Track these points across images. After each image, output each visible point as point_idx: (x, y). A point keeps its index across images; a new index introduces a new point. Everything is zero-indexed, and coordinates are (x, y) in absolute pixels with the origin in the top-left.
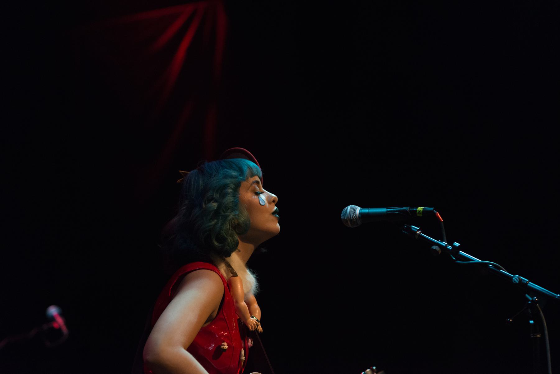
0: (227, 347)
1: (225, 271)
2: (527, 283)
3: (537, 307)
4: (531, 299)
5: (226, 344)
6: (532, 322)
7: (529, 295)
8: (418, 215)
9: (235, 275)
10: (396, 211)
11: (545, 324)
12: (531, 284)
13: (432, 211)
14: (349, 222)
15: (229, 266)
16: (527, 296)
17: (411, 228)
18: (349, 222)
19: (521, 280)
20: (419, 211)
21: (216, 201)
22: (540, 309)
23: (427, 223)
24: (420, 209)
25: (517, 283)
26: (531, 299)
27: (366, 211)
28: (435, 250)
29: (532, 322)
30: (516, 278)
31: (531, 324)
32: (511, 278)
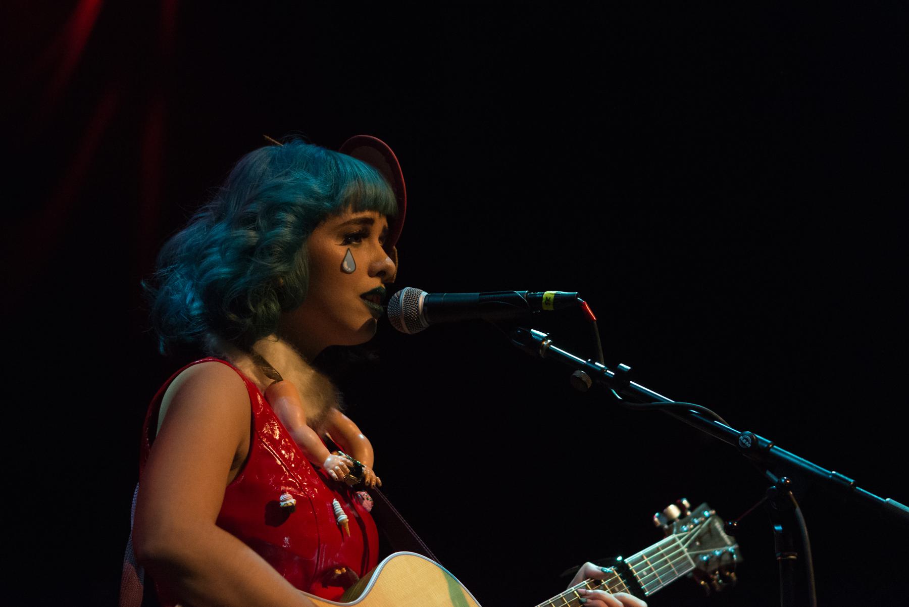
0: (293, 501)
1: (254, 372)
2: (768, 448)
3: (789, 496)
4: (776, 480)
5: (288, 495)
6: (778, 528)
7: (773, 473)
8: (545, 308)
9: (279, 379)
10: (500, 299)
11: (806, 532)
12: (778, 450)
13: (572, 299)
14: (403, 322)
15: (261, 362)
16: (769, 473)
17: (531, 334)
18: (403, 322)
19: (755, 442)
20: (548, 299)
21: (257, 229)
22: (794, 501)
23: (562, 321)
24: (549, 294)
25: (747, 448)
26: (776, 480)
27: (443, 297)
28: (580, 379)
29: (778, 528)
30: (746, 437)
31: (777, 531)
32: (735, 438)
